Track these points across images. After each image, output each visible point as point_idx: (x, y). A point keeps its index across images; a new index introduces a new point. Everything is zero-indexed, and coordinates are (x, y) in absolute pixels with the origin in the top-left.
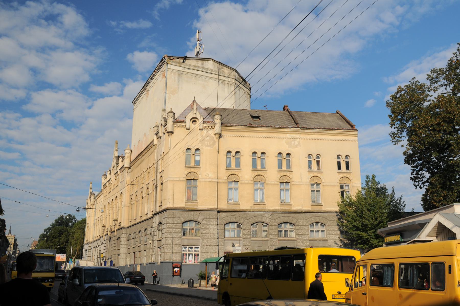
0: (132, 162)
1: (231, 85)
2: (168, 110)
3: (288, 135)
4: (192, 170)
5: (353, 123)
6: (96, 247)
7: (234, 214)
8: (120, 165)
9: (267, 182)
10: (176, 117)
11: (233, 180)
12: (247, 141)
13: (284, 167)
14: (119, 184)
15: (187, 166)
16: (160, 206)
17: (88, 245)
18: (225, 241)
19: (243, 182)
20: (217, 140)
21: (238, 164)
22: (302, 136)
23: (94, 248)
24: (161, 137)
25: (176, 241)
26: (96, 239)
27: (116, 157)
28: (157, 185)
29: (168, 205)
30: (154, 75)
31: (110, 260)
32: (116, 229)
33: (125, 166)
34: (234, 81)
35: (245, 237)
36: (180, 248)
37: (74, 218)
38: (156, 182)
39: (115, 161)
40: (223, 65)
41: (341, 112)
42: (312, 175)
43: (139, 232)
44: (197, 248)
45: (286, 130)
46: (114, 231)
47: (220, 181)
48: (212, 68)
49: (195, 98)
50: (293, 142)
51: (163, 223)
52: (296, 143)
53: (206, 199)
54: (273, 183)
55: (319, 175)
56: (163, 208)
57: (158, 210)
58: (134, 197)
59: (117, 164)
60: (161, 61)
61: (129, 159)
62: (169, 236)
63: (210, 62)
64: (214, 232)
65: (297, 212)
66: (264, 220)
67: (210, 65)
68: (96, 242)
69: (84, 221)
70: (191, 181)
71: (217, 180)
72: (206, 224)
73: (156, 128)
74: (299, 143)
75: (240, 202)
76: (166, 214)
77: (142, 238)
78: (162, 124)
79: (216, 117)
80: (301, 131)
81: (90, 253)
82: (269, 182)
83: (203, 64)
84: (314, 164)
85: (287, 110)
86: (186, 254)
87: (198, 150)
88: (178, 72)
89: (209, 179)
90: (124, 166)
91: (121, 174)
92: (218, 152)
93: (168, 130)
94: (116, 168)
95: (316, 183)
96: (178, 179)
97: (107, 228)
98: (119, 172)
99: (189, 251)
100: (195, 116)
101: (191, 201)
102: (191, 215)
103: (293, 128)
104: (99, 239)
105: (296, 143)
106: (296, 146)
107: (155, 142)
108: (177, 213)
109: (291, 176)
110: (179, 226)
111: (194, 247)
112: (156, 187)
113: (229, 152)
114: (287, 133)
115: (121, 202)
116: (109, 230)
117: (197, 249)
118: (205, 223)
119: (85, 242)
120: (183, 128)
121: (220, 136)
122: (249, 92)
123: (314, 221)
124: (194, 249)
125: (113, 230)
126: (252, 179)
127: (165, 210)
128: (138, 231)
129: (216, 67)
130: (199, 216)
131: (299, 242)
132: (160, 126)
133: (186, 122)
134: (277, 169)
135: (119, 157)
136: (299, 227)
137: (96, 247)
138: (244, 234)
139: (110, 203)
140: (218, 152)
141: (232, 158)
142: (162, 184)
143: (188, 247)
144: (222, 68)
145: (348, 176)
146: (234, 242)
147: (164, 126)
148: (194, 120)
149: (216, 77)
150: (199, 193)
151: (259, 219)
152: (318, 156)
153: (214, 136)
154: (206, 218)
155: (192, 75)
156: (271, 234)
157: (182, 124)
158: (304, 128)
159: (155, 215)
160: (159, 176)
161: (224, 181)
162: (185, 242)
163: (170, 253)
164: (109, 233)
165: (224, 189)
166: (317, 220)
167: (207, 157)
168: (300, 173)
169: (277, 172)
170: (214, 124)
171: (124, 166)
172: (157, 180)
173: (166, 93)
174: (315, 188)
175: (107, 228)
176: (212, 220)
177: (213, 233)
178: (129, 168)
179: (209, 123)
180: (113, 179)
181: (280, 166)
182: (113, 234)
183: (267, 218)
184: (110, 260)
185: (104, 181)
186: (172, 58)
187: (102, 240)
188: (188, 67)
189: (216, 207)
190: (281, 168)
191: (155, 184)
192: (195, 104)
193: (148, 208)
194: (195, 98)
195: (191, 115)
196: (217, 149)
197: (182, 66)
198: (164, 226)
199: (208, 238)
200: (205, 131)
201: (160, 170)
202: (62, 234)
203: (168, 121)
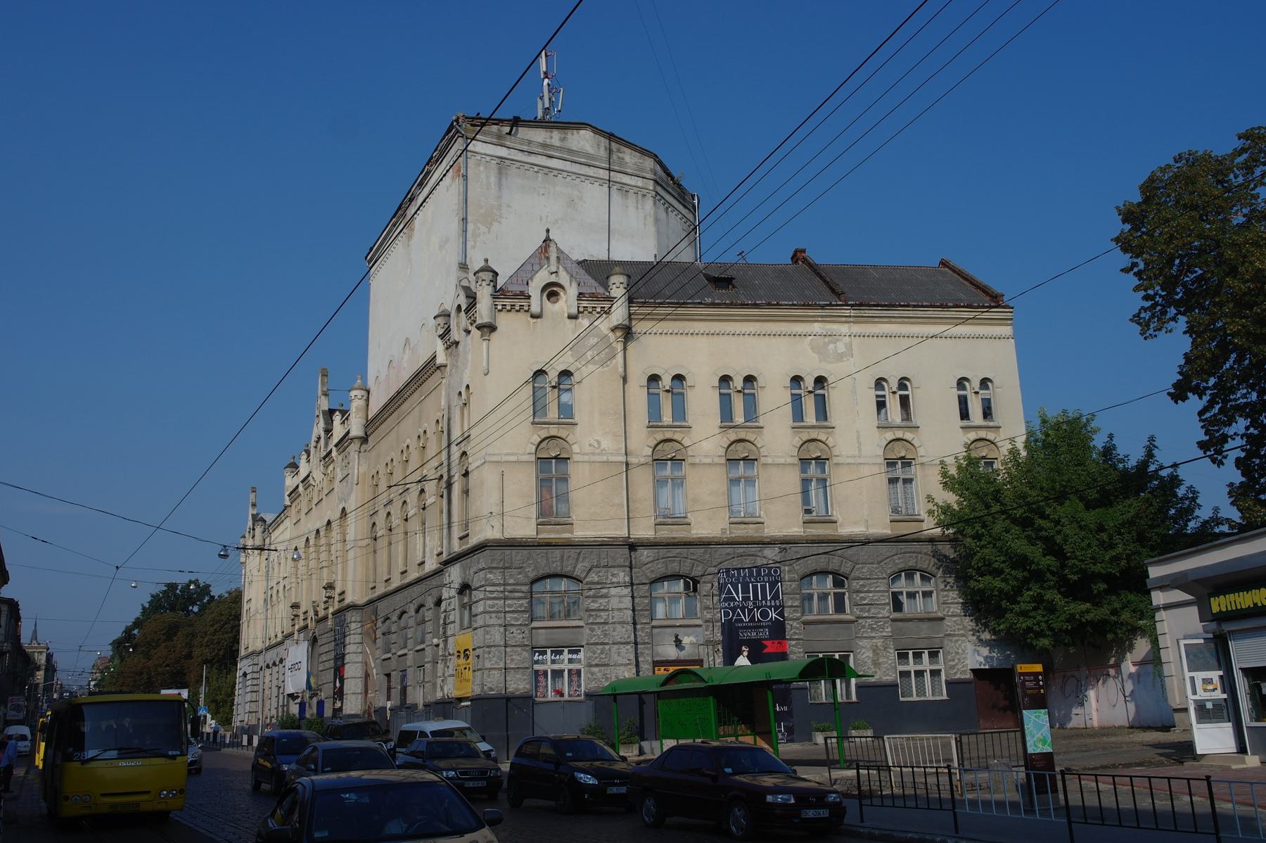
0: (372, 425)
1: (644, 196)
2: (477, 264)
3: (817, 327)
4: (553, 431)
5: (997, 288)
6: (274, 664)
7: (675, 551)
8: (338, 431)
9: (763, 460)
10: (501, 282)
11: (668, 458)
12: (700, 349)
13: (810, 417)
14: (336, 484)
15: (537, 420)
16: (461, 539)
17: (248, 662)
18: (655, 631)
19: (697, 461)
20: (620, 346)
21: (680, 411)
22: (856, 329)
23: (268, 667)
24: (457, 343)
25: (517, 636)
26: (274, 641)
27: (324, 412)
28: (450, 477)
29: (486, 531)
30: (428, 173)
31: (315, 700)
32: (331, 610)
33: (352, 434)
34: (651, 185)
35: (709, 616)
36: (526, 654)
37: (205, 589)
38: (449, 470)
39: (322, 424)
40: (621, 141)
41: (955, 262)
42: (890, 435)
43: (400, 618)
44: (577, 652)
45: (811, 312)
46: (325, 618)
47: (632, 460)
48: (591, 151)
49: (548, 231)
50: (831, 346)
51: (475, 584)
53: (595, 513)
54: (782, 461)
55: (908, 436)
56: (473, 541)
57: (457, 547)
58: (380, 519)
59: (328, 431)
60: (449, 131)
61: (362, 414)
62: (493, 621)
63: (582, 132)
65: (852, 542)
67: (584, 140)
68: (275, 651)
69: (236, 598)
70: (552, 465)
71: (623, 459)
72: (598, 583)
73: (441, 320)
75: (691, 518)
76: (482, 560)
77: (410, 633)
78: (459, 307)
79: (614, 279)
80: (853, 313)
81: (255, 682)
82: (770, 460)
84: (893, 405)
85: (805, 260)
86: (545, 673)
87: (566, 374)
88: (498, 161)
90: (348, 433)
91: (340, 458)
92: (625, 379)
93: (479, 321)
94: (326, 444)
95: (903, 458)
96: (514, 458)
97: (303, 609)
98: (334, 454)
99: (553, 662)
100: (553, 279)
101: (553, 520)
102: (554, 560)
103: (830, 305)
104: (281, 643)
105: (841, 347)
106: (840, 357)
107: (441, 359)
108: (518, 555)
109: (830, 442)
111: (566, 650)
112: (449, 486)
113: (654, 379)
114: (813, 320)
115: (344, 534)
116: (311, 613)
117: (575, 656)
118: (596, 579)
119: (243, 653)
120: (522, 315)
121: (627, 333)
122: (690, 216)
123: (901, 566)
124: (566, 656)
125: (322, 613)
126: (722, 452)
127: (481, 547)
128: (398, 612)
129: (602, 149)
130: (577, 559)
131: (863, 627)
132: (453, 314)
133: (529, 297)
134: (789, 421)
135: (331, 412)
136: (862, 582)
137: (274, 664)
138: (707, 608)
139: (312, 542)
140: (625, 379)
141: (663, 395)
142: (466, 474)
143: (549, 651)
144: (619, 151)
145: (991, 436)
146: (680, 631)
147: (467, 311)
148: (552, 292)
149: (603, 174)
150: (573, 496)
152: (903, 384)
153: (611, 334)
155: (536, 169)
157: (518, 304)
158: (861, 305)
159: (447, 563)
160: (456, 452)
161: (643, 460)
162: (541, 638)
163: (500, 669)
164: (311, 625)
165: (643, 481)
166: (911, 563)
167: (593, 395)
168: (856, 434)
169: (790, 431)
170: (611, 299)
171: (348, 433)
172: (449, 465)
173: (465, 220)
174: (899, 472)
175: (303, 609)
176: (615, 571)
177: (620, 609)
178: (364, 440)
179: (594, 297)
180: (317, 475)
181: (798, 414)
182: (321, 625)
184: (315, 700)
185: (290, 482)
186: (480, 122)
188: (525, 148)
189: (624, 533)
190: (802, 420)
191: (445, 477)
192: (552, 249)
193: (427, 549)
194: (548, 231)
195: (542, 277)
196: (621, 370)
197: (508, 143)
198: (477, 595)
199: (606, 623)
200: (584, 322)
201: (456, 434)
202: (175, 634)
203: (479, 295)
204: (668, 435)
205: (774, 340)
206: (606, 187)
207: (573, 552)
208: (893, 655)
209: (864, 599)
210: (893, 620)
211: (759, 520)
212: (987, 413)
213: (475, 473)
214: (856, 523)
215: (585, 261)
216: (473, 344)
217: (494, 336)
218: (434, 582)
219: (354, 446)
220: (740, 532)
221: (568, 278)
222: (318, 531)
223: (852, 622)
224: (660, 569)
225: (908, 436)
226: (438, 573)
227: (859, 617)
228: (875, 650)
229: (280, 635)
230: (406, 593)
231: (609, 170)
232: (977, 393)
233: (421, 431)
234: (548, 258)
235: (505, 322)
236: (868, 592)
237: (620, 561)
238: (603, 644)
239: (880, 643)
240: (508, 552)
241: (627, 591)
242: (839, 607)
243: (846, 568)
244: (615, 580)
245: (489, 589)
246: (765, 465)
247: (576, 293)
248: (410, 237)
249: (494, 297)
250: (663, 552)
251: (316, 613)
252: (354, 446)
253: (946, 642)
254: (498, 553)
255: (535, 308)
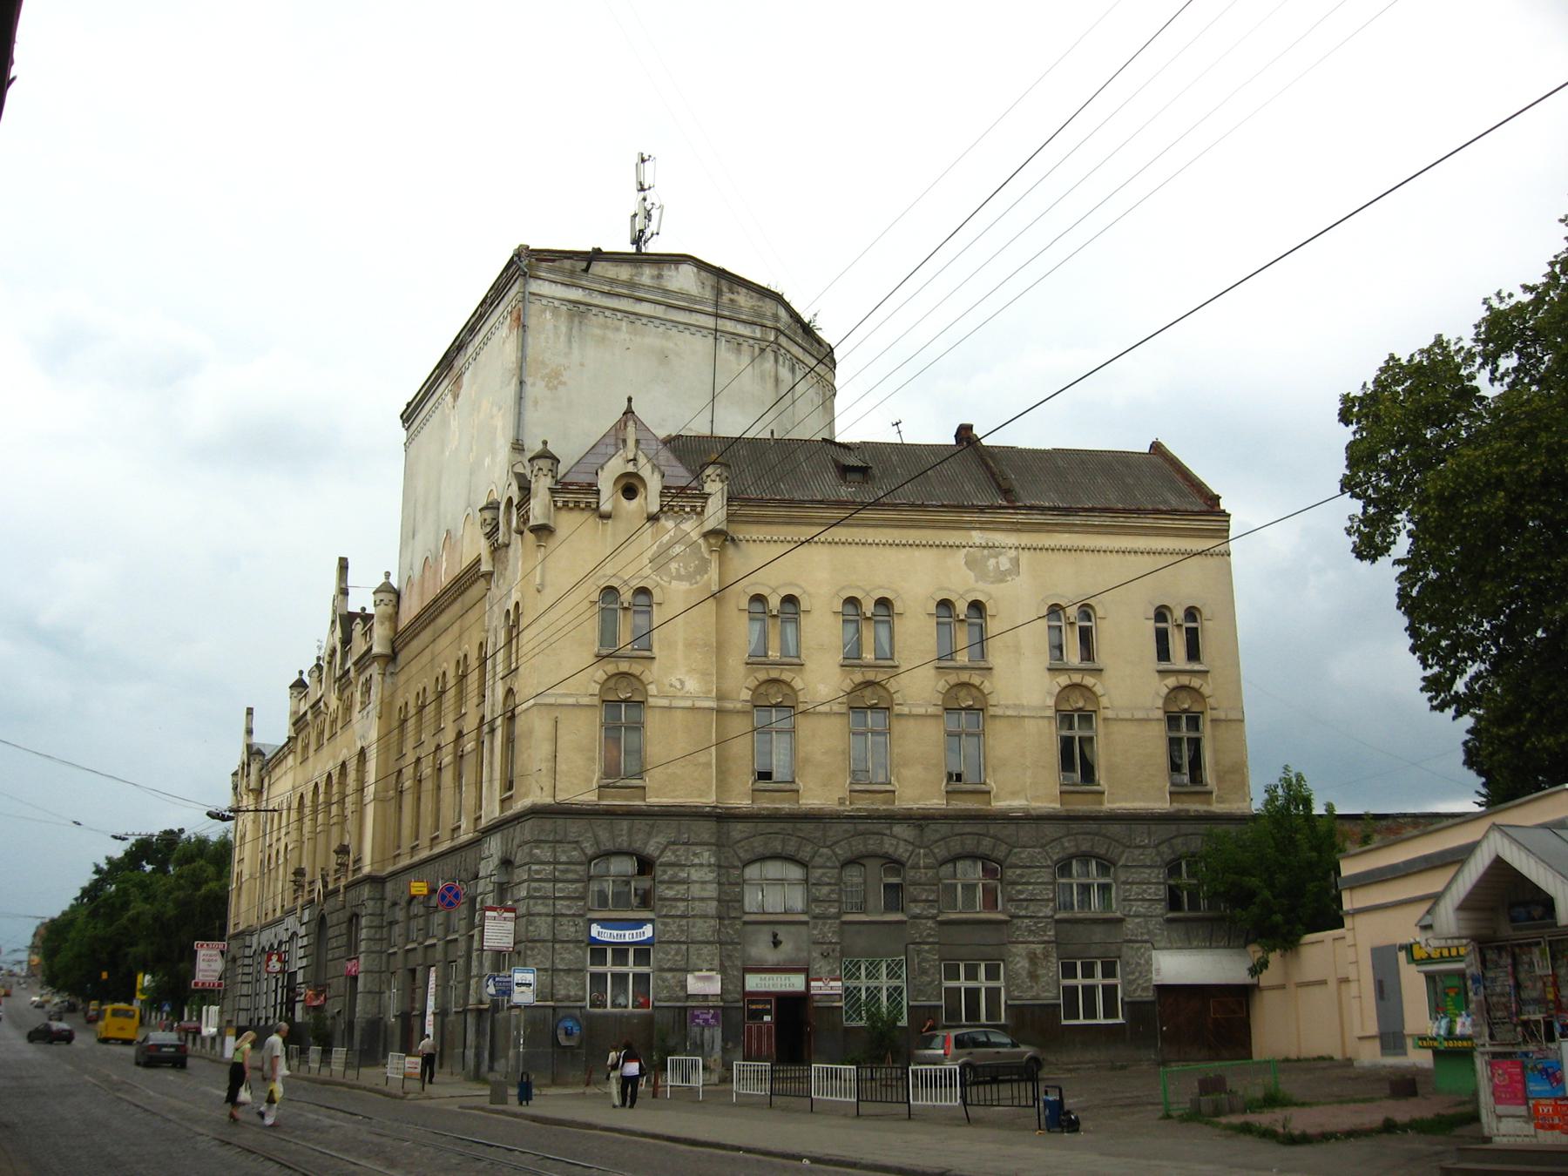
1: (762, 350)
3: (977, 537)
8: (358, 646)
10: (562, 469)
18: (750, 928)
24: (507, 546)
33: (376, 650)
46: (336, 891)
49: (630, 400)
50: (992, 562)
51: (518, 860)
52: (1005, 563)
53: (679, 774)
54: (922, 711)
56: (519, 806)
64: (705, 894)
65: (1005, 818)
66: (888, 846)
70: (623, 706)
73: (488, 515)
74: (1016, 562)
76: (526, 830)
78: (510, 499)
82: (906, 710)
83: (660, 276)
88: (570, 306)
89: (683, 697)
93: (532, 522)
96: (571, 701)
98: (352, 674)
100: (630, 468)
102: (623, 834)
105: (1005, 563)
106: (1001, 577)
107: (485, 567)
108: (574, 828)
110: (575, 872)
116: (319, 885)
118: (673, 859)
120: (587, 514)
129: (708, 289)
131: (1018, 928)
136: (1018, 871)
147: (519, 507)
149: (709, 322)
151: (872, 845)
153: (701, 541)
154: (674, 843)
156: (915, 901)
157: (584, 499)
166: (1085, 847)
168: (1023, 680)
175: (308, 878)
176: (698, 849)
177: (702, 899)
183: (898, 841)
187: (291, 922)
189: (709, 799)
194: (630, 400)
195: (616, 466)
204: (774, 674)
205: (917, 553)
206: (711, 339)
207: (640, 824)
208: (1054, 966)
209: (1020, 892)
210: (1058, 921)
211: (888, 787)
212: (1193, 653)
213: (523, 717)
214: (1014, 794)
215: (679, 437)
216: (520, 551)
217: (553, 543)
218: (470, 854)
219: (375, 670)
220: (864, 804)
221: (649, 467)
222: (330, 776)
223: (1005, 922)
224: (758, 846)
225: (1089, 681)
226: (475, 843)
227: (1013, 917)
228: (1033, 958)
229: (278, 913)
230: (437, 865)
231: (717, 316)
232: (1179, 626)
233: (461, 655)
234: (624, 441)
235: (567, 523)
236: (1028, 883)
237: (706, 837)
238: (678, 942)
239: (1039, 948)
240: (560, 822)
241: (711, 876)
242: (990, 903)
243: (1001, 852)
244: (696, 861)
245: (534, 867)
246: (899, 715)
247: (659, 487)
248: (458, 381)
249: (552, 491)
250: (762, 826)
251: (325, 885)
252: (375, 670)
253: (1124, 949)
254: (548, 824)
255: (606, 507)
